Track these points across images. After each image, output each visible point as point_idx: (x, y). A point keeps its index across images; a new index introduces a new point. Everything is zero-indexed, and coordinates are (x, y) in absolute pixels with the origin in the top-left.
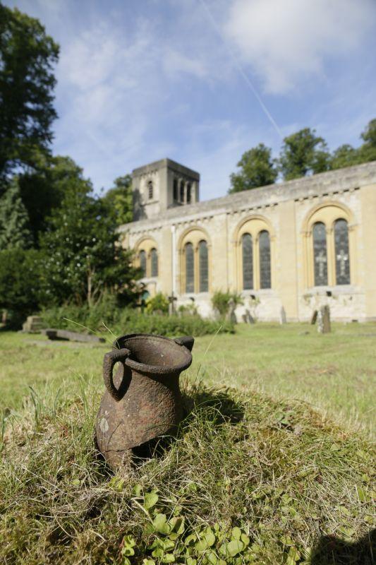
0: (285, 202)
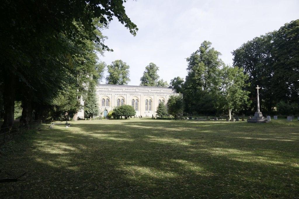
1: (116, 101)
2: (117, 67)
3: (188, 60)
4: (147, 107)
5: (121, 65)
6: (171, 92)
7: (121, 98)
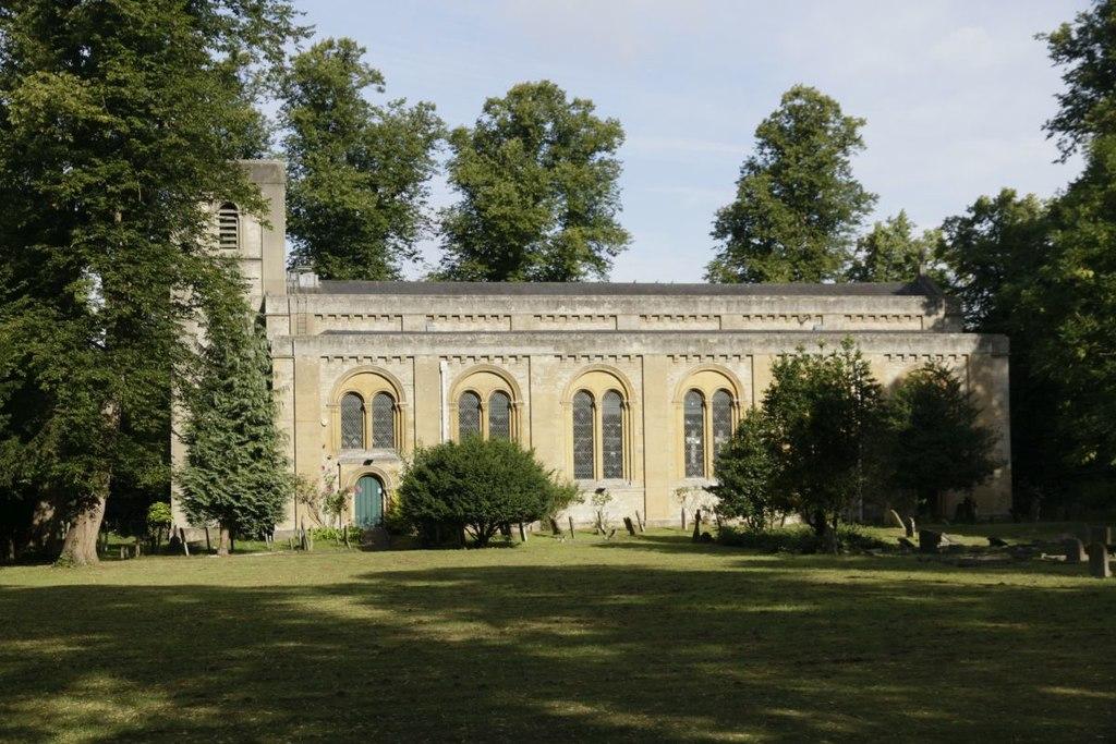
0: (653, 355)
1: (446, 408)
2: (513, 144)
3: (1063, 46)
4: (700, 447)
5: (549, 127)
6: (915, 325)
7: (486, 385)
